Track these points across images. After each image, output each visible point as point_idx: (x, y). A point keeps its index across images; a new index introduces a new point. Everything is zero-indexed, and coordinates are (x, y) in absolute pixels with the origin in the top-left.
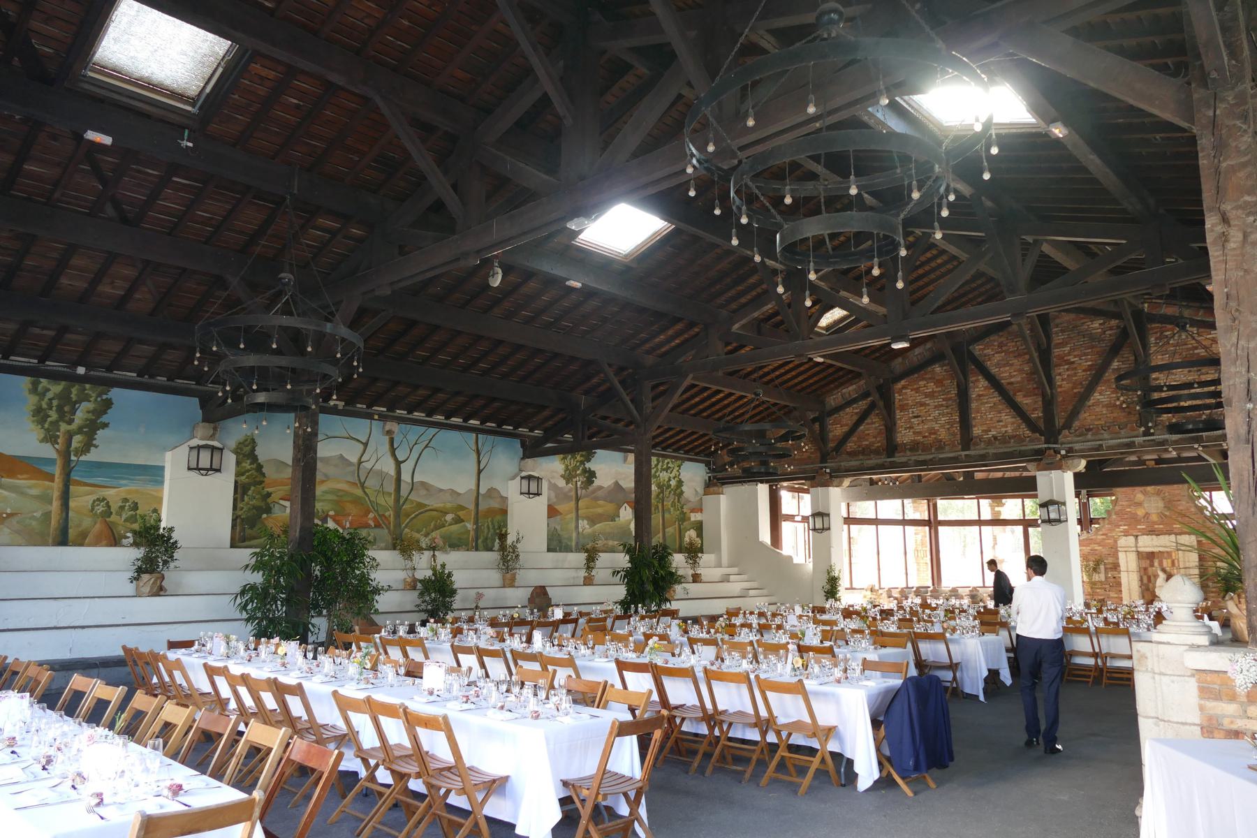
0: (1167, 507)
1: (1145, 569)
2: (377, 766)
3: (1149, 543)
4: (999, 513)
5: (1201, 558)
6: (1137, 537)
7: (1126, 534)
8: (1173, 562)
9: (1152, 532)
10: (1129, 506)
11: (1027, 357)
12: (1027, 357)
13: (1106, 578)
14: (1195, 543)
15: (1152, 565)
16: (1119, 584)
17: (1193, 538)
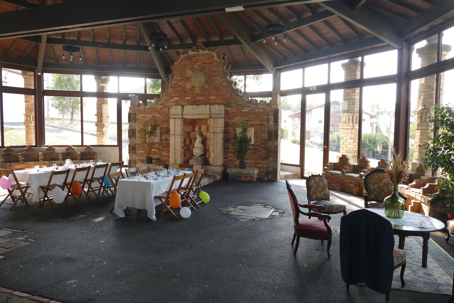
0: (207, 82)
1: (189, 133)
2: (162, 201)
3: (192, 112)
4: (103, 88)
5: (226, 125)
6: (183, 106)
7: (177, 103)
8: (208, 127)
9: (195, 103)
10: (181, 81)
11: (353, 162)
12: (353, 162)
13: (161, 140)
14: (223, 112)
15: (194, 130)
16: (168, 145)
17: (222, 107)
